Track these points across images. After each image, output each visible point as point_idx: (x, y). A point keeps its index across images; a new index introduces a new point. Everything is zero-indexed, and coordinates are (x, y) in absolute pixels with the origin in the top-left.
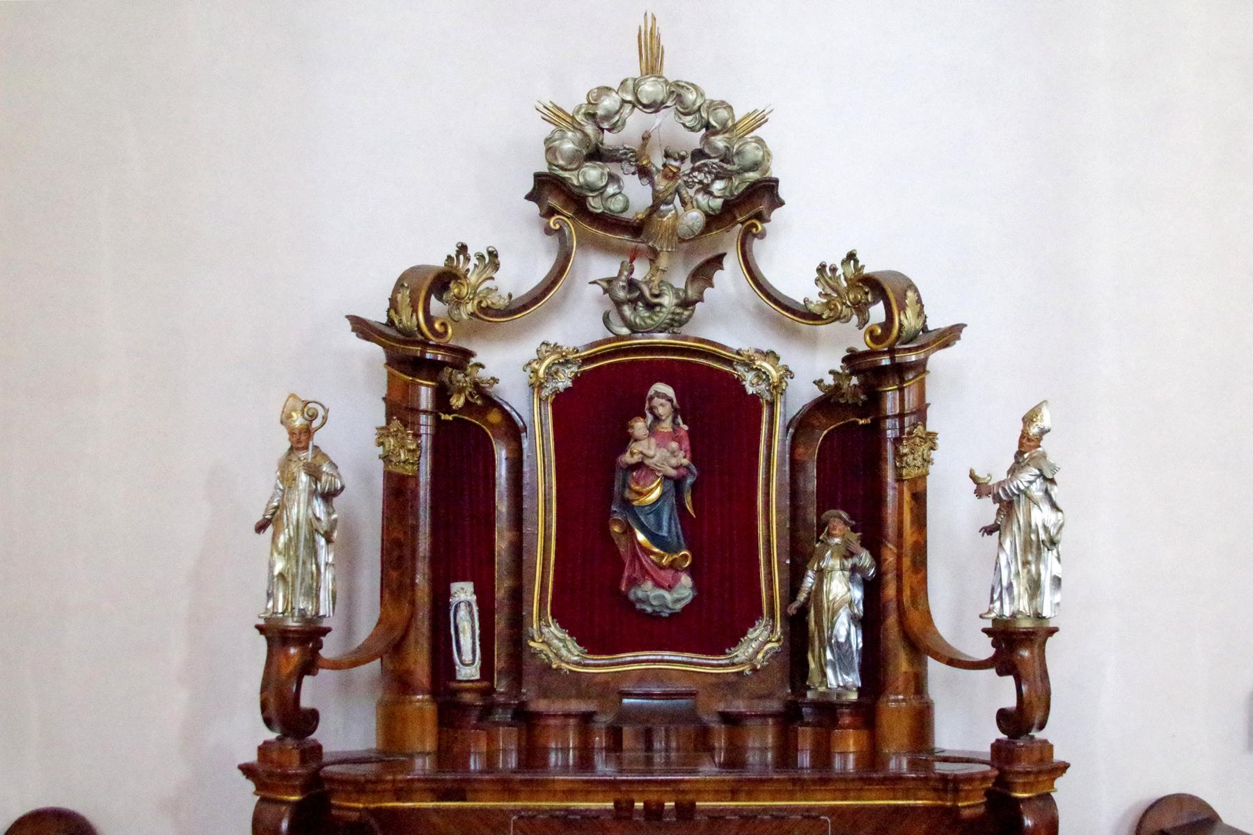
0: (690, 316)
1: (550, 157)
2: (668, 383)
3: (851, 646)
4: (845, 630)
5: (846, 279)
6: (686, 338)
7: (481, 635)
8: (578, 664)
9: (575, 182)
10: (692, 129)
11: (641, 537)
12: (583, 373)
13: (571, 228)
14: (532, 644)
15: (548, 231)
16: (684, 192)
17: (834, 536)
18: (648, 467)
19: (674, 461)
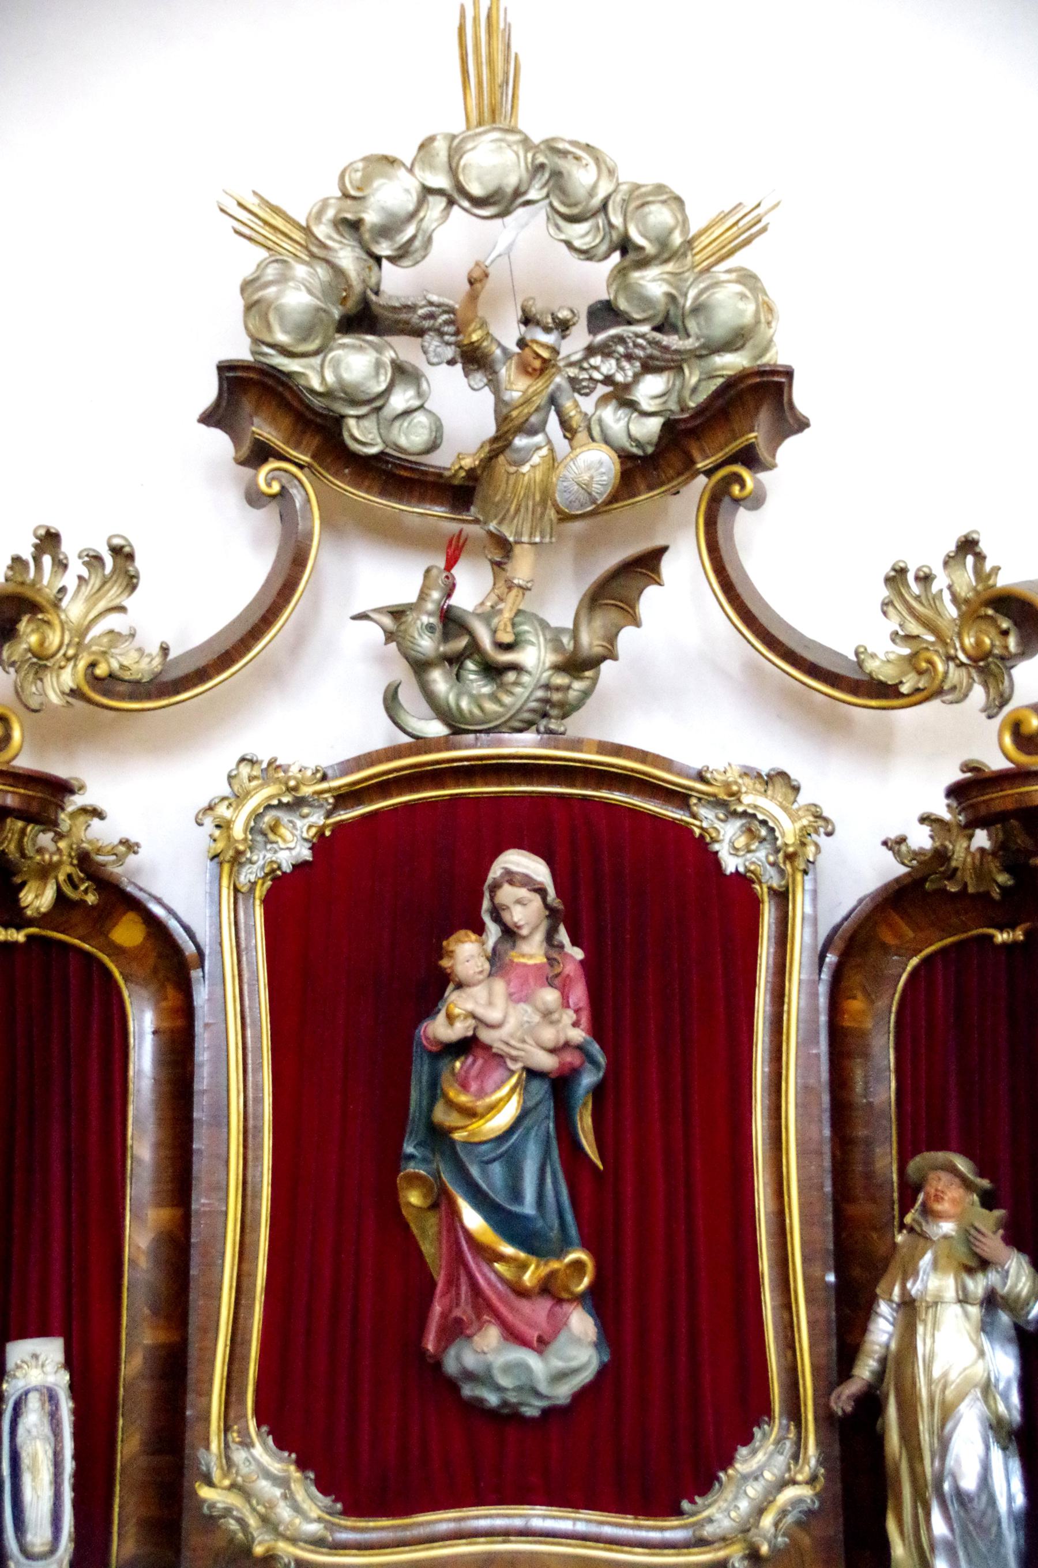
0: (587, 694)
1: (254, 323)
2: (536, 849)
3: (992, 1501)
5: (955, 599)
6: (577, 744)
7: (77, 1475)
8: (318, 1543)
9: (316, 384)
10: (587, 254)
11: (473, 1220)
12: (339, 827)
13: (306, 492)
14: (205, 1492)
15: (254, 498)
16: (568, 404)
17: (938, 1216)
18: (488, 1048)
19: (549, 1035)
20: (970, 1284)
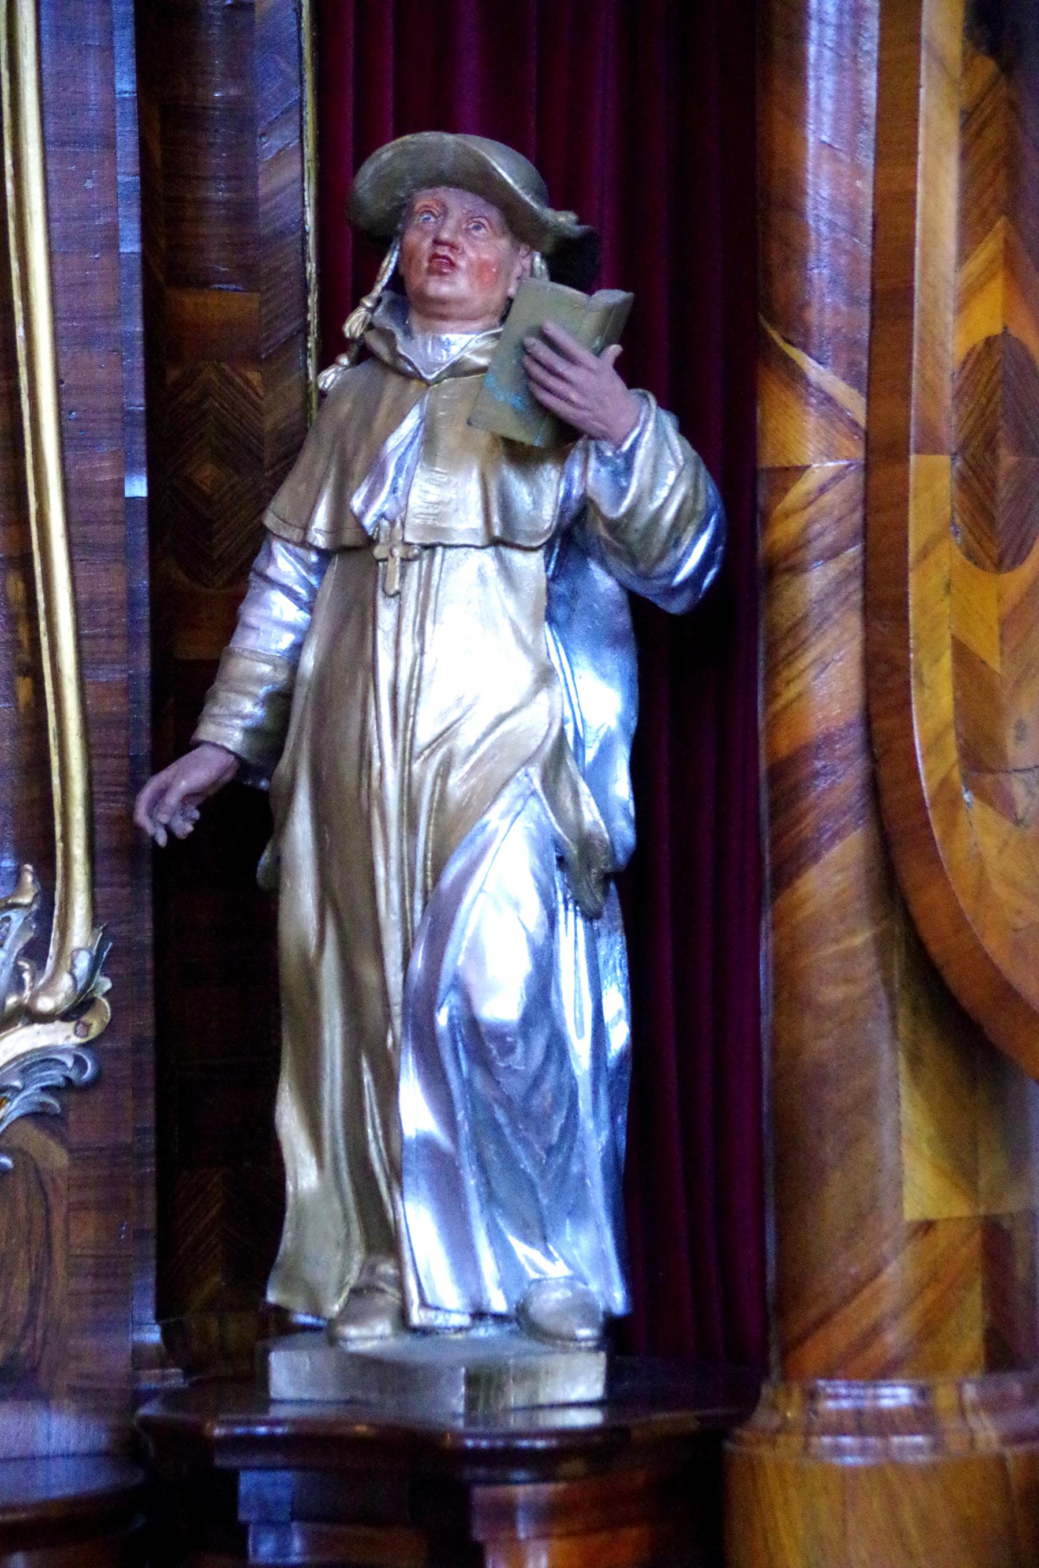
3: (557, 1047)
4: (520, 944)
17: (438, 312)
20: (521, 493)
